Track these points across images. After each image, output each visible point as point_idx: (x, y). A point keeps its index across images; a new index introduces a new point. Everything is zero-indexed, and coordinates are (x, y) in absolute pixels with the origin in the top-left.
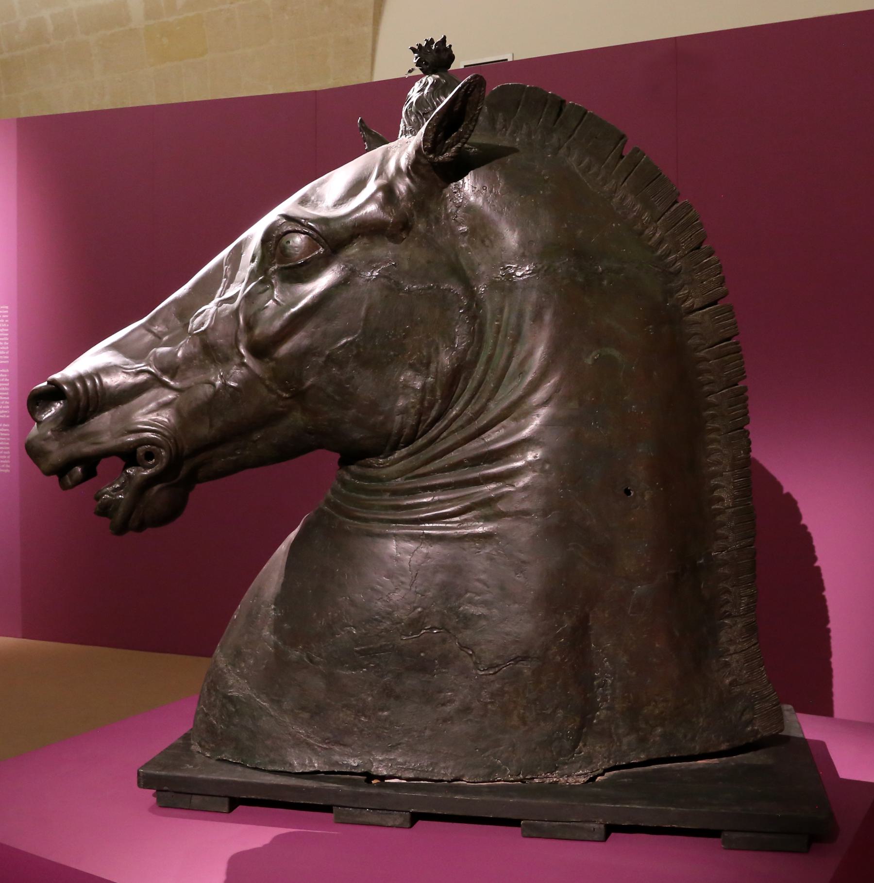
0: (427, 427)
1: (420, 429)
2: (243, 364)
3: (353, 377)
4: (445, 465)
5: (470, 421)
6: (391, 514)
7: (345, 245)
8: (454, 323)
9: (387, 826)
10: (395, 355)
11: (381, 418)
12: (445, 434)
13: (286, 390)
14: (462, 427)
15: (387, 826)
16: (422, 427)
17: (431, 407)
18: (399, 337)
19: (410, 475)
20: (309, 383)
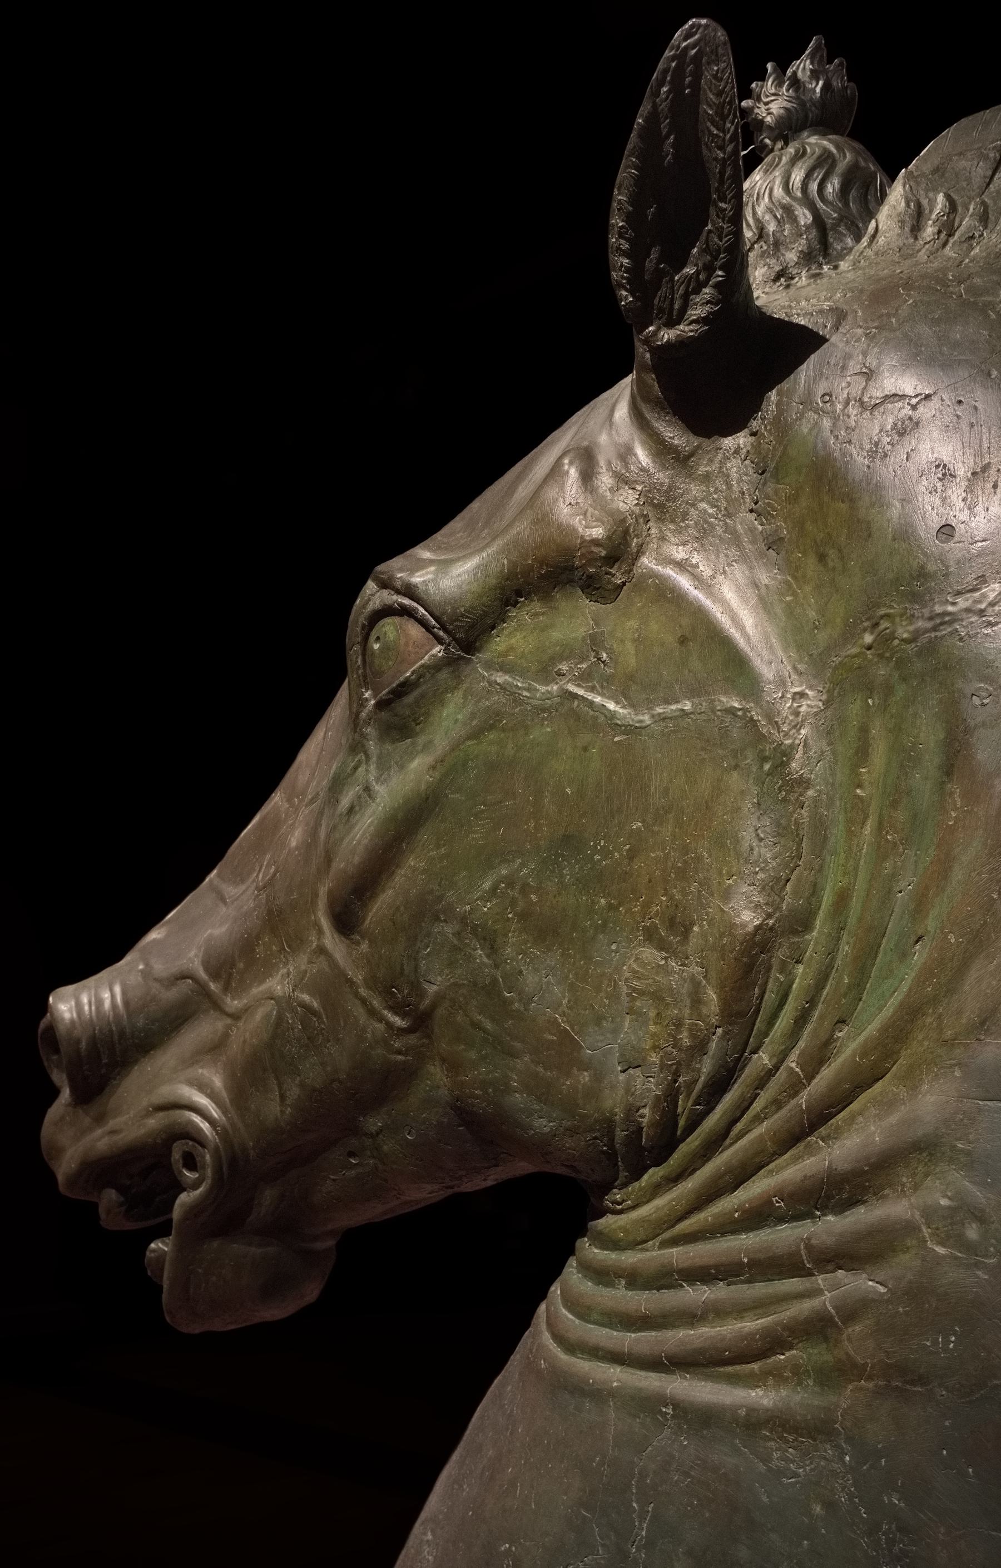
0: (697, 1103)
1: (679, 1110)
2: (322, 950)
3: (520, 972)
4: (745, 1204)
5: (795, 1087)
6: (827, 900)
7: (493, 628)
8: (686, 454)
9: (749, 1309)
10: (610, 907)
11: (585, 1077)
12: (739, 1126)
13: (397, 1009)
14: (777, 1104)
15: (749, 1309)
16: (685, 1106)
17: (700, 1047)
18: (958, 1218)
19: (667, 1235)
20: (432, 989)
